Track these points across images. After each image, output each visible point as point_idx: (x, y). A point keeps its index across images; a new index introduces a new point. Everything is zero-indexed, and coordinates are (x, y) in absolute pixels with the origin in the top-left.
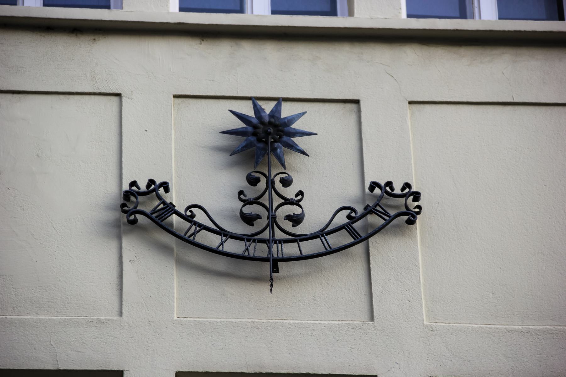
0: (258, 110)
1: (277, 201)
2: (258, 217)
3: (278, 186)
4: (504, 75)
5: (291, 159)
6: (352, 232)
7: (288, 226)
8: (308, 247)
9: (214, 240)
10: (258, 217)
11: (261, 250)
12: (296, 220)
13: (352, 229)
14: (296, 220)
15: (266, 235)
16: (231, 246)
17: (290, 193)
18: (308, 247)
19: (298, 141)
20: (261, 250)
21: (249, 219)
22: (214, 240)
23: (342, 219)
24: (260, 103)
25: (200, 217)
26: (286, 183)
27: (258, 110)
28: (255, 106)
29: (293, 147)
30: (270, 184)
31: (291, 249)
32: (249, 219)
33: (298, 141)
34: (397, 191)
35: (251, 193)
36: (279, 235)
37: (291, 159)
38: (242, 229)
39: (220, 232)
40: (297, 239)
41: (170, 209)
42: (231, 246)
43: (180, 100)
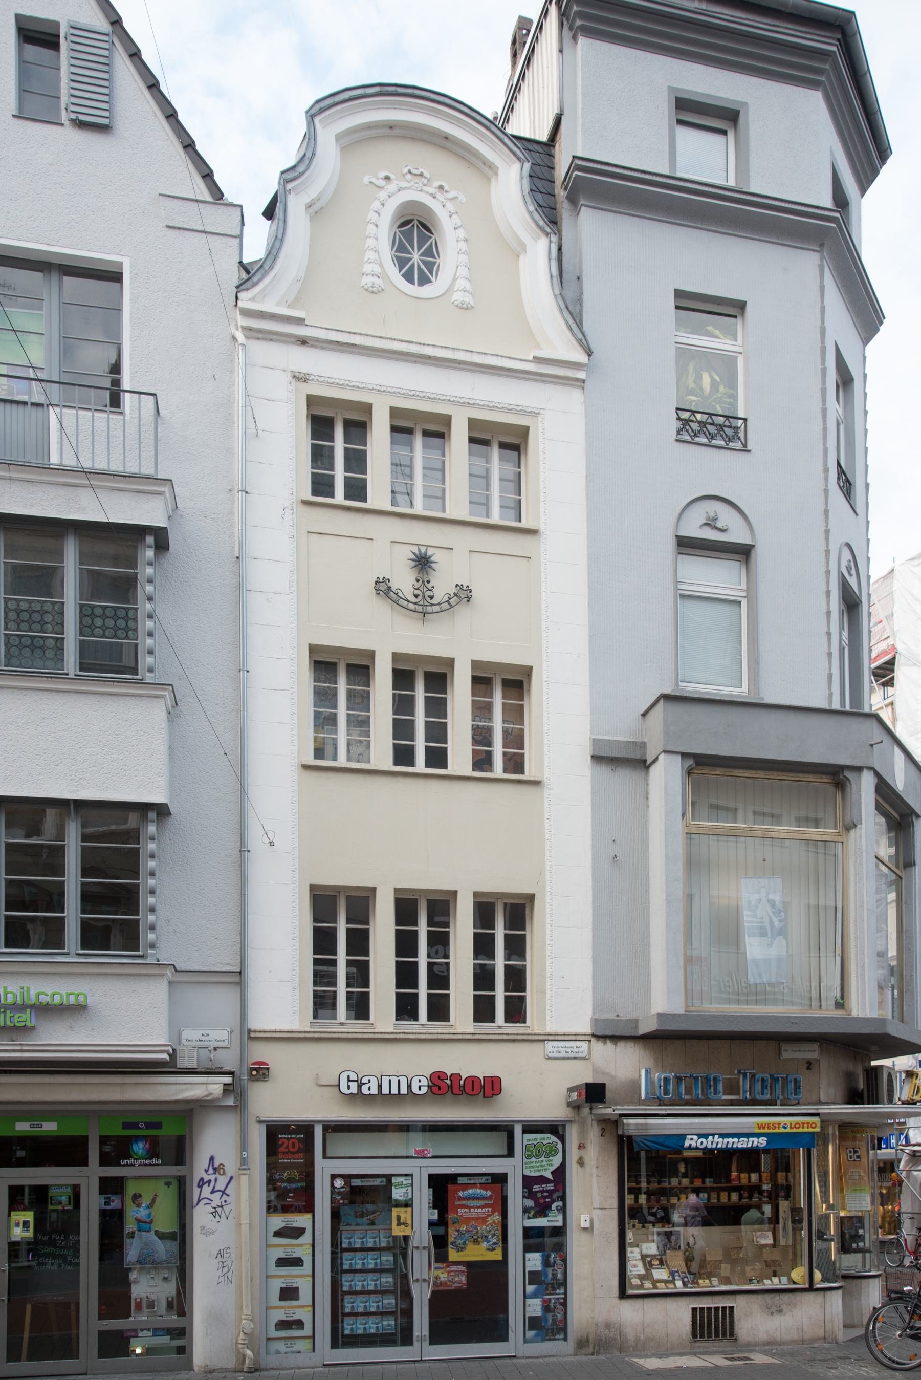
0: (420, 551)
1: (426, 589)
2: (419, 595)
3: (426, 583)
4: (831, 151)
5: (430, 571)
6: (450, 604)
7: (428, 599)
8: (436, 608)
9: (404, 603)
10: (419, 595)
11: (420, 609)
12: (431, 598)
13: (701, 54)
14: (431, 598)
15: (421, 603)
16: (411, 606)
17: (430, 586)
18: (436, 608)
19: (433, 565)
20: (420, 609)
21: (416, 596)
22: (404, 603)
23: (446, 598)
24: (420, 547)
25: (400, 594)
26: (428, 582)
27: (420, 551)
28: (419, 549)
29: (430, 567)
30: (423, 582)
31: (429, 609)
32: (416, 596)
33: (433, 565)
34: (464, 588)
35: (417, 585)
36: (426, 603)
37: (430, 571)
38: (413, 599)
39: (408, 601)
40: (432, 605)
41: (389, 588)
42: (411, 606)
43: (172, 232)
